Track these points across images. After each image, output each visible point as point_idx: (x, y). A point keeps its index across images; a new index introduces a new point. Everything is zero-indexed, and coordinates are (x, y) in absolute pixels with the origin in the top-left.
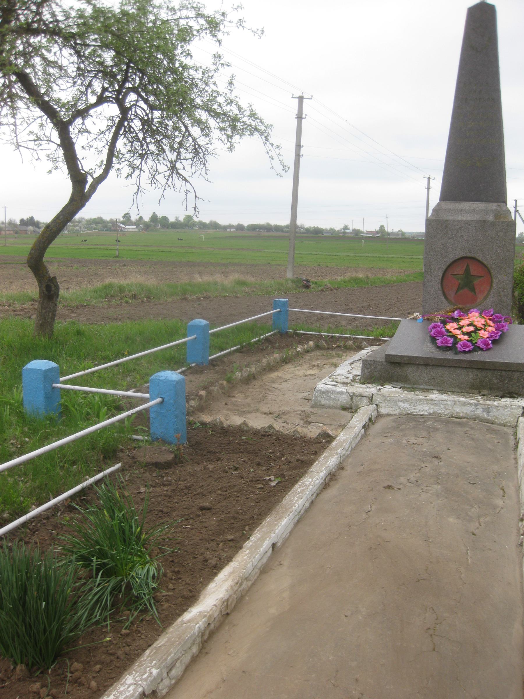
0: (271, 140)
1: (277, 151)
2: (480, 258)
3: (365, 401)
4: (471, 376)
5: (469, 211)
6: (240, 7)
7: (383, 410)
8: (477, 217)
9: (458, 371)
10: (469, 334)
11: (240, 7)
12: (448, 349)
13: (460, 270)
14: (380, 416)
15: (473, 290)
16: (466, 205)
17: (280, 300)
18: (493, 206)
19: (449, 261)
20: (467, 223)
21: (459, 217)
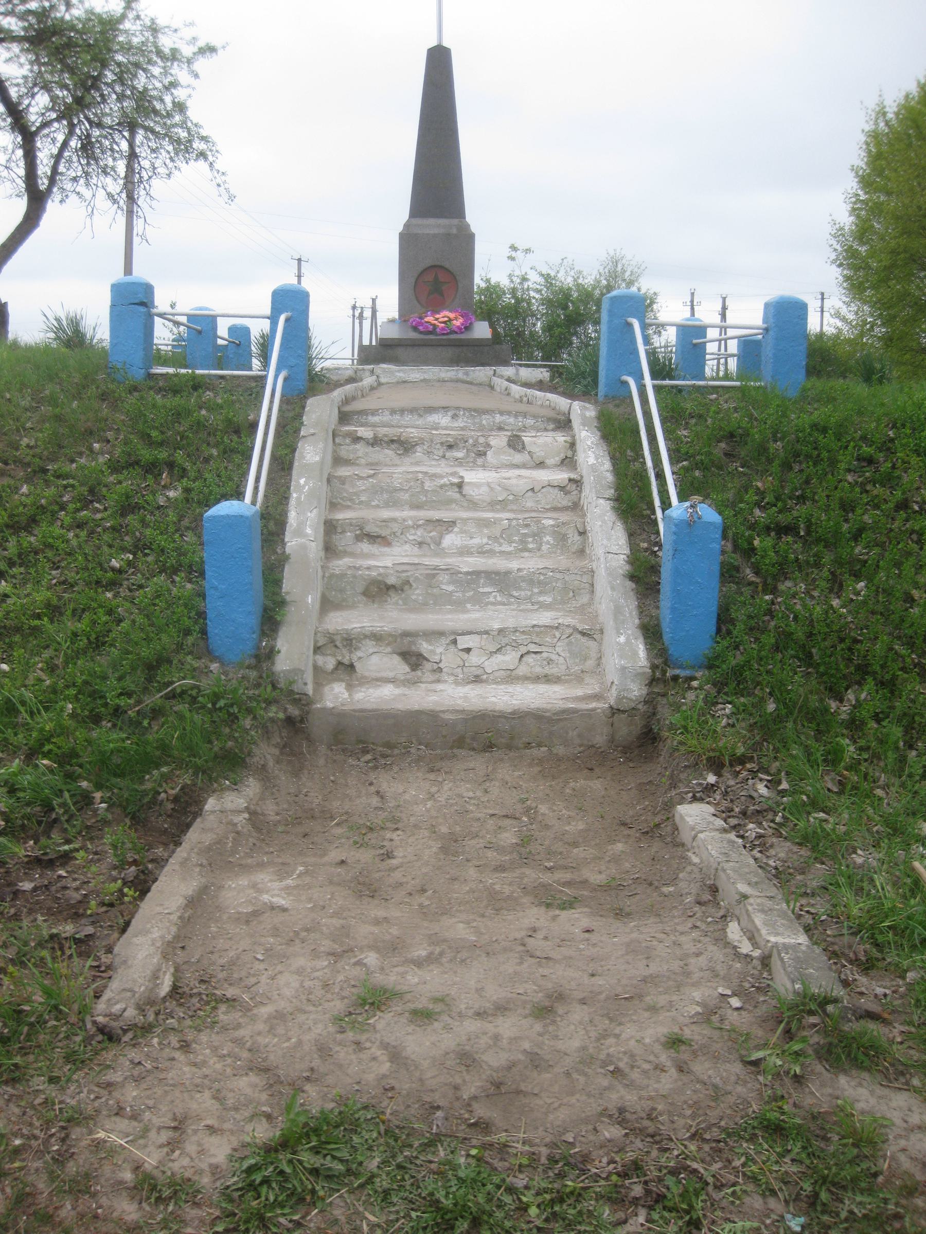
0: (216, 166)
1: (223, 178)
2: (447, 266)
3: (368, 373)
4: (449, 352)
5: (433, 226)
6: (192, 24)
7: (383, 380)
8: (442, 231)
9: (440, 349)
10: (444, 322)
11: (192, 24)
12: (430, 333)
13: (430, 277)
14: (380, 384)
15: (442, 294)
16: (432, 221)
17: (206, 372)
18: (455, 221)
19: (420, 269)
20: (435, 236)
21: (427, 231)
